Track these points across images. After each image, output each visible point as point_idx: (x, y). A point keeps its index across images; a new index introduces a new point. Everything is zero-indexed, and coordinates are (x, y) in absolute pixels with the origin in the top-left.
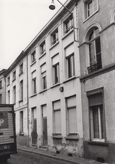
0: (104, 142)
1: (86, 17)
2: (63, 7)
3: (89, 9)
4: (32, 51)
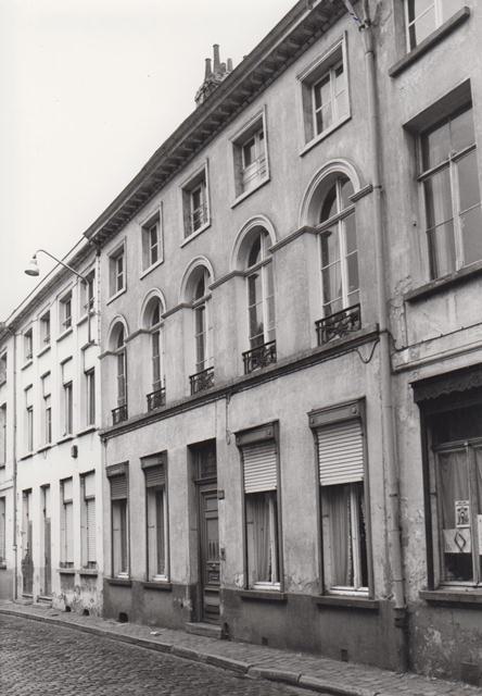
0: (366, 597)
1: (113, 293)
2: (61, 267)
3: (410, 21)
4: (24, 328)
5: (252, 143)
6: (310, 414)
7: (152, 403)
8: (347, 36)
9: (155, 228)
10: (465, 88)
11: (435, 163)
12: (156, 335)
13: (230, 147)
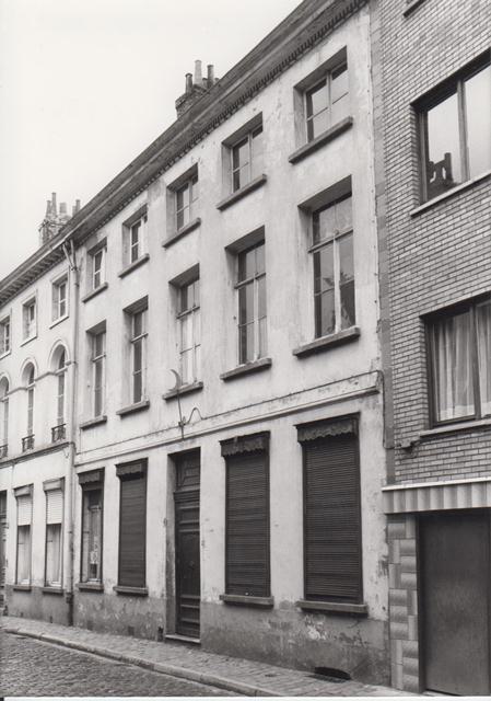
5: (139, 224)
6: (44, 483)
7: (56, 436)
8: (354, 38)
9: (64, 286)
10: (347, 182)
11: (324, 240)
12: (31, 391)
13: (21, 307)
